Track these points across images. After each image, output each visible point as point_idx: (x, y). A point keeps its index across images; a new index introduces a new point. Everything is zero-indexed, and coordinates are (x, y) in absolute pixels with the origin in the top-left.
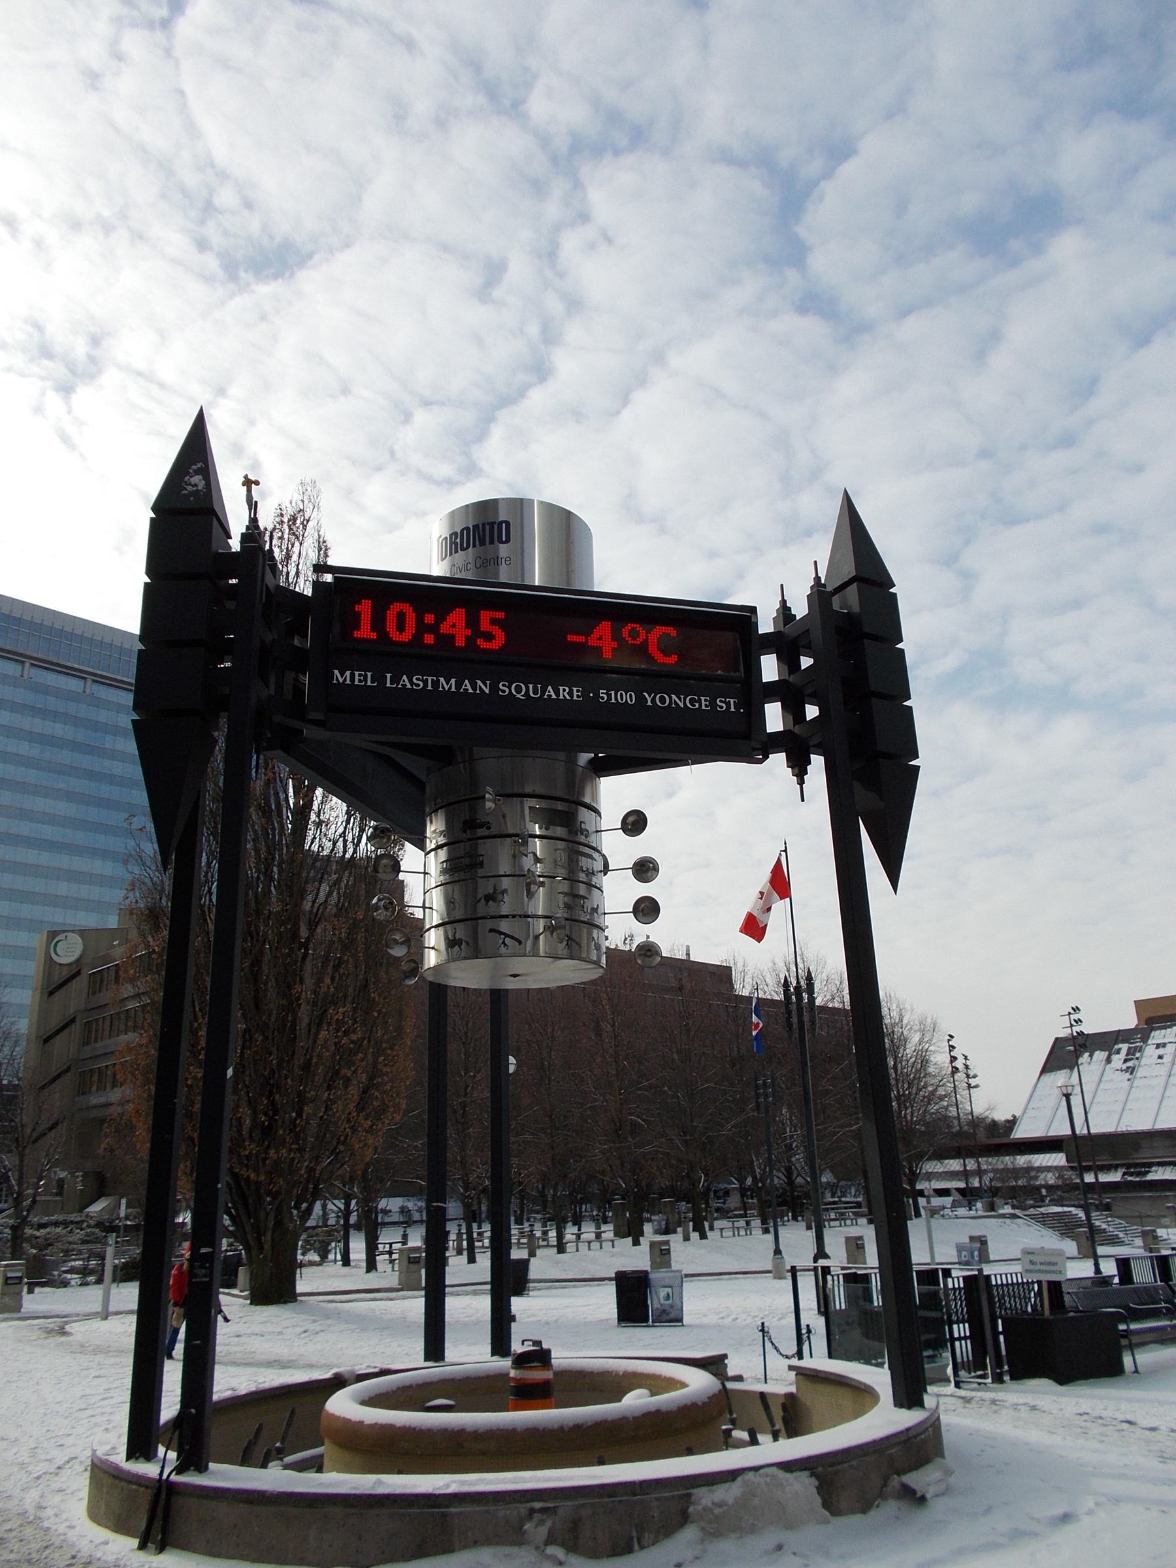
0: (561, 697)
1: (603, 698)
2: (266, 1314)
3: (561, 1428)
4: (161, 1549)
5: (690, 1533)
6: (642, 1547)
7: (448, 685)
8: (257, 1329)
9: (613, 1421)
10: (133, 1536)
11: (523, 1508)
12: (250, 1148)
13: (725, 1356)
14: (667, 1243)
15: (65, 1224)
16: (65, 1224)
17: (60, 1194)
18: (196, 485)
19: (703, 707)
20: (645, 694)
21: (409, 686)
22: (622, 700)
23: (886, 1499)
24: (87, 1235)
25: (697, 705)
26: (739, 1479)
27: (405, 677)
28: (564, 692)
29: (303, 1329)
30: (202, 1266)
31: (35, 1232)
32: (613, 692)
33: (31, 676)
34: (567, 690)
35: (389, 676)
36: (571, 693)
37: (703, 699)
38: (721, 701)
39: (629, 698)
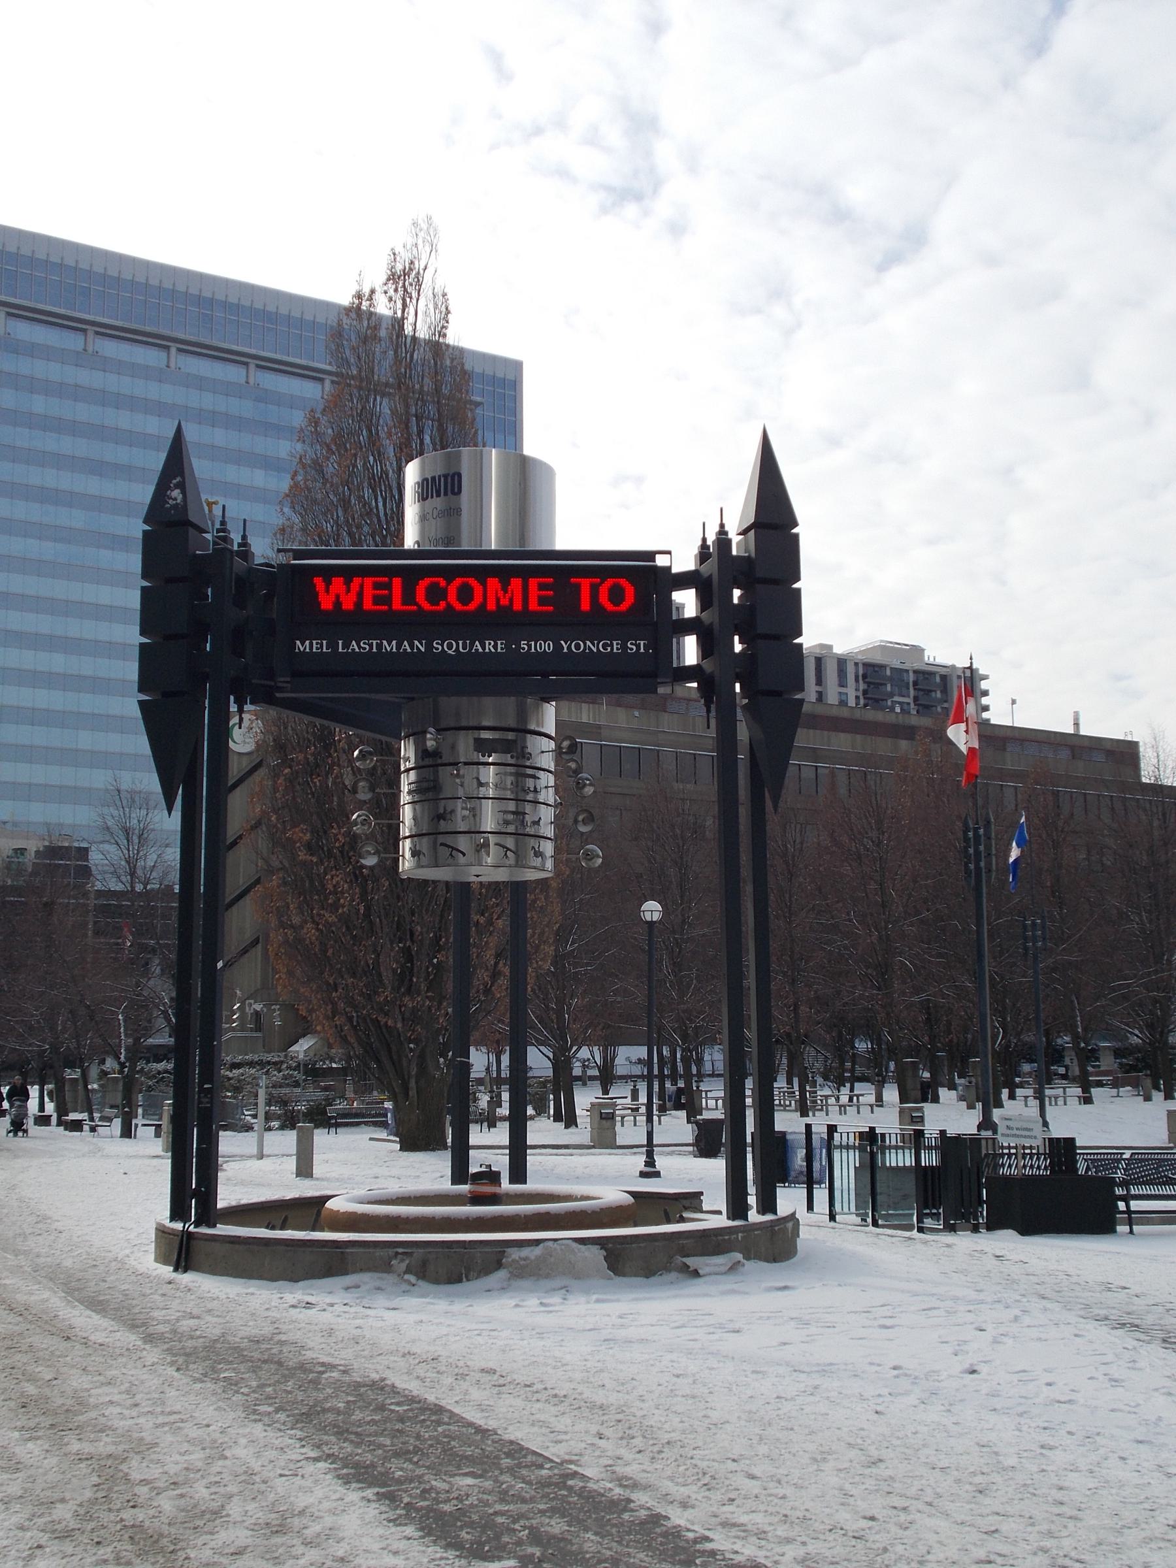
0: (487, 650)
1: (524, 649)
2: (411, 1160)
3: (467, 1218)
4: (185, 1271)
5: (502, 1274)
6: (468, 1280)
7: (390, 647)
8: (395, 1172)
9: (508, 1217)
10: (169, 1265)
11: (391, 1252)
12: (386, 994)
13: (702, 1193)
14: (920, 1109)
15: (261, 1064)
16: (261, 1064)
17: (258, 1028)
18: (175, 499)
19: (615, 651)
20: (562, 642)
21: (357, 650)
22: (541, 649)
23: (670, 1271)
24: (285, 1077)
25: (609, 649)
26: (542, 1245)
27: (354, 643)
28: (489, 646)
29: (439, 1174)
30: (206, 1096)
31: (228, 1073)
32: (533, 643)
33: (179, 366)
34: (493, 643)
35: (340, 642)
36: (495, 647)
37: (615, 643)
38: (631, 644)
39: (547, 646)
